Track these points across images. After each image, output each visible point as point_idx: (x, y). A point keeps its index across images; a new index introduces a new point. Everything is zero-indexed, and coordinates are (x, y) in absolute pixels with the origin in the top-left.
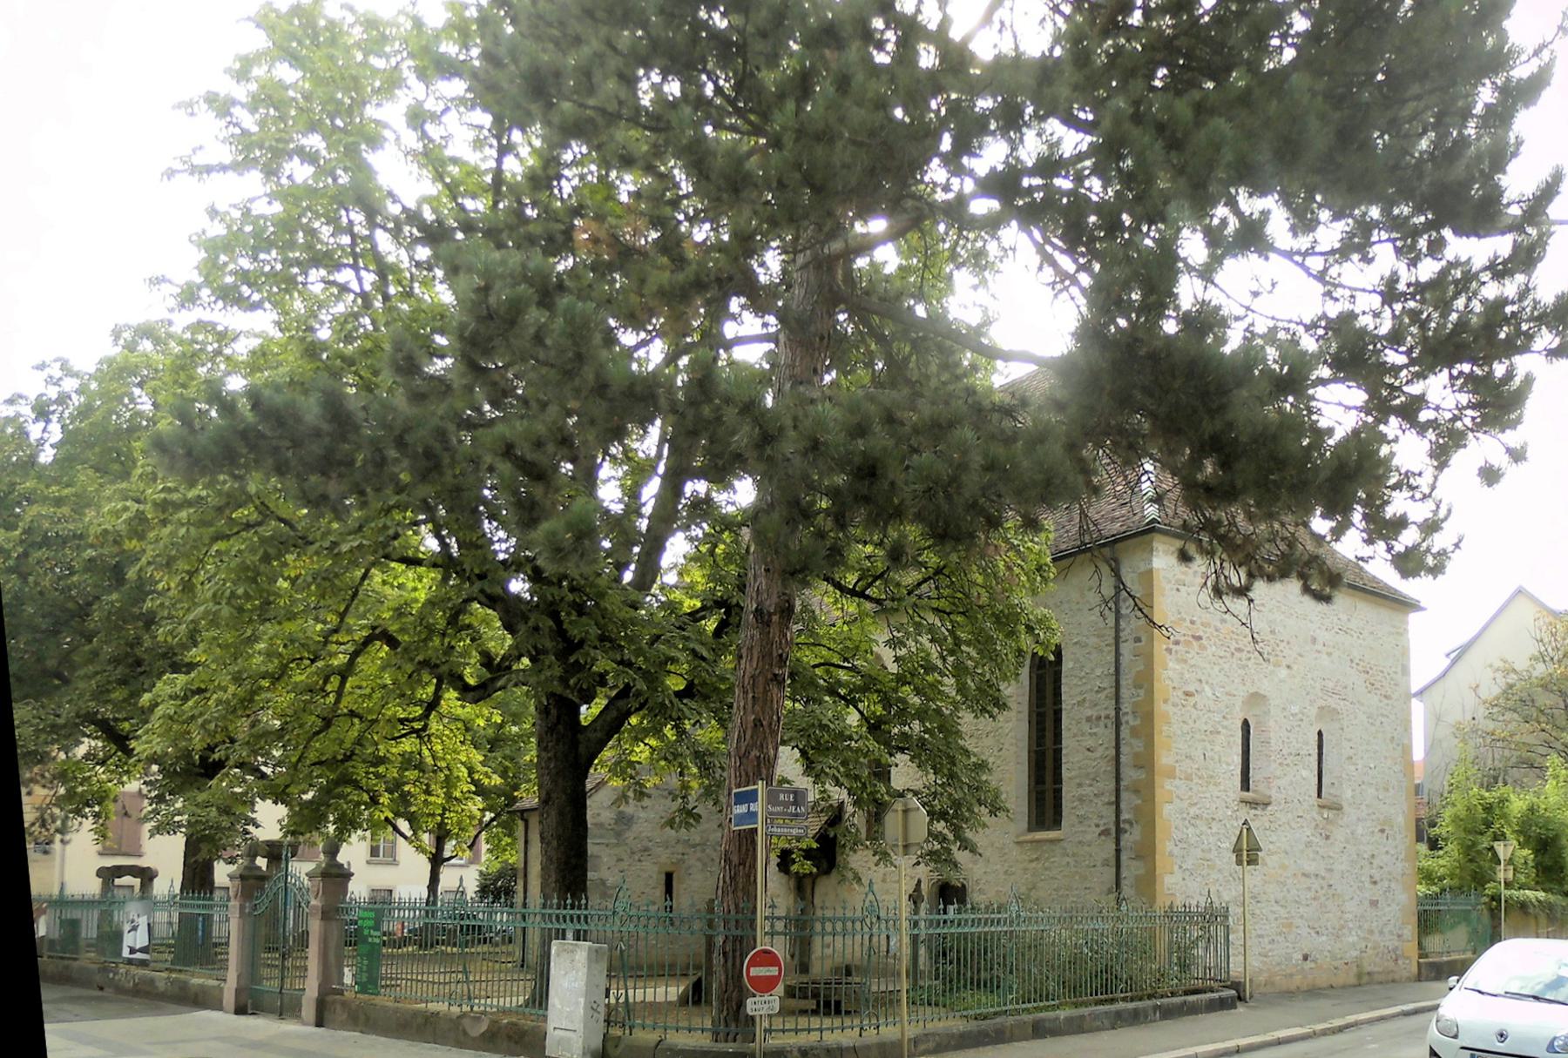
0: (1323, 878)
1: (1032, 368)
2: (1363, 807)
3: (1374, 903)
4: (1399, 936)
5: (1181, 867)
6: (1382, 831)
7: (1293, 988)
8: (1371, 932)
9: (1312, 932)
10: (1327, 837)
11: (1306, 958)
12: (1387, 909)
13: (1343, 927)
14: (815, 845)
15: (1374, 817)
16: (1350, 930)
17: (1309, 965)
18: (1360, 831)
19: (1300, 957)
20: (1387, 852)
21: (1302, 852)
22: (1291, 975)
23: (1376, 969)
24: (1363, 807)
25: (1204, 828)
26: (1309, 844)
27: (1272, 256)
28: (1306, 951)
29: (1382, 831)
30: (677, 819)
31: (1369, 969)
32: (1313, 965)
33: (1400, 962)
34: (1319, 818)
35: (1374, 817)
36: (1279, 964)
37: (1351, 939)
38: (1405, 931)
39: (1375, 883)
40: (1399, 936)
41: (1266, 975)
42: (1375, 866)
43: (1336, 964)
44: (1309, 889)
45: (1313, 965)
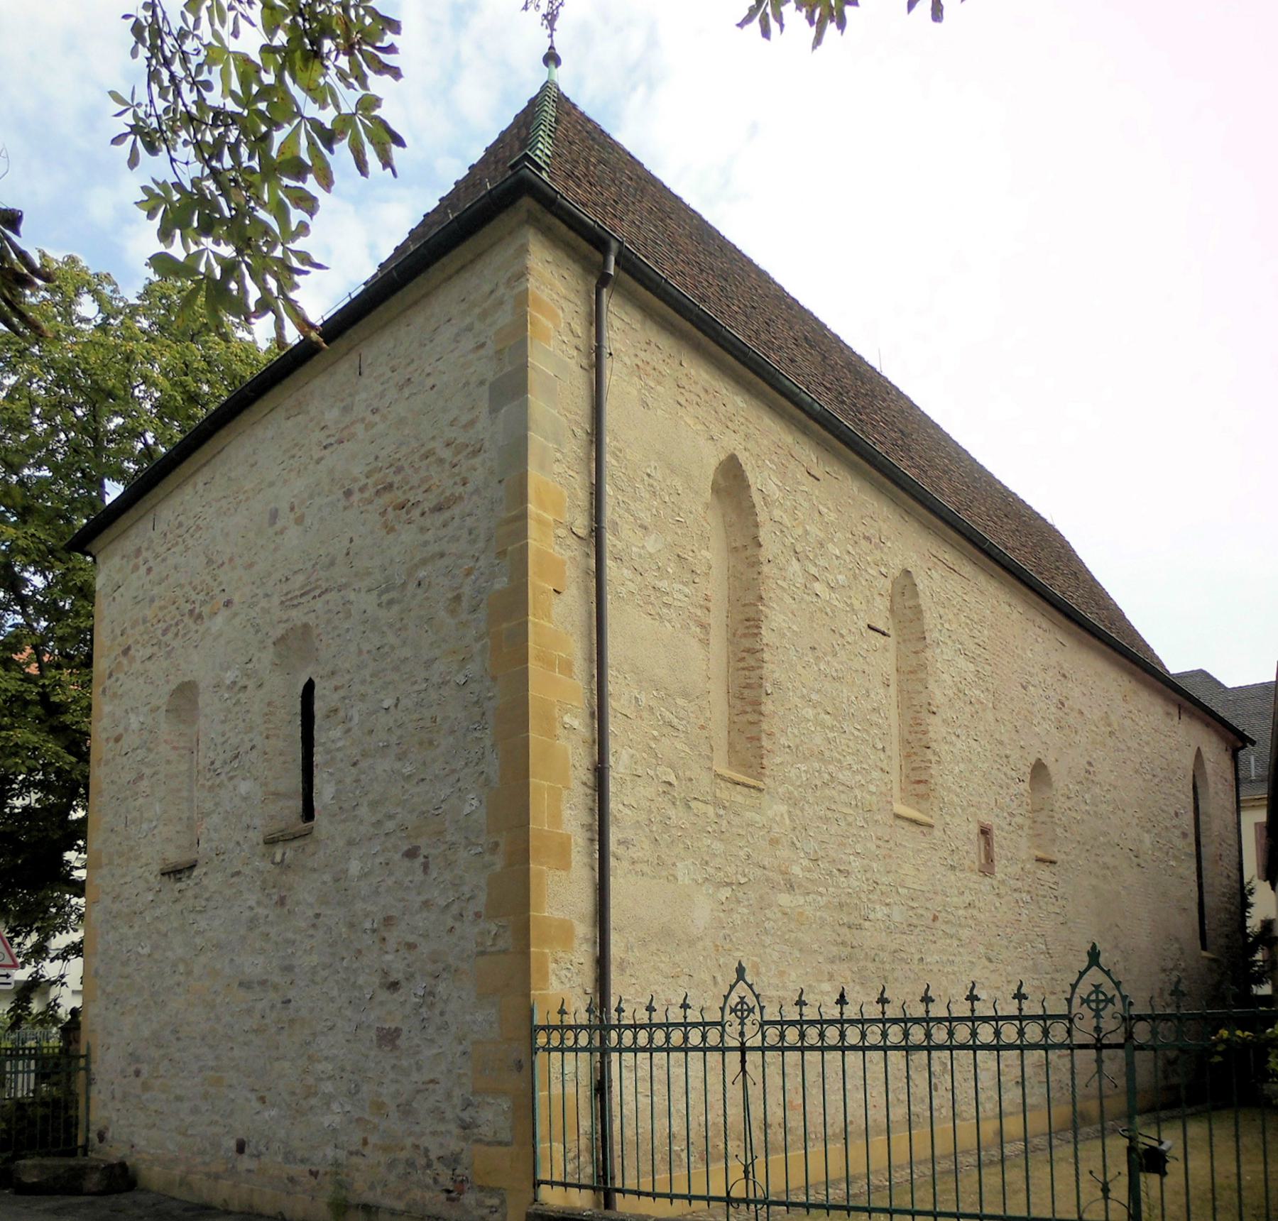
0: (276, 987)
1: (152, 84)
2: (364, 811)
3: (389, 1038)
4: (465, 1126)
5: (104, 991)
6: (411, 854)
7: (217, 1201)
8: (379, 1107)
9: (253, 1097)
10: (282, 902)
11: (241, 1147)
12: (428, 1052)
13: (310, 1093)
14: (1270, 1050)
15: (390, 825)
16: (328, 1099)
17: (245, 1163)
18: (355, 867)
19: (232, 1144)
20: (426, 904)
21: (243, 938)
22: (217, 1177)
23: (388, 1202)
24: (364, 811)
25: (125, 930)
26: (252, 923)
27: (129, 129)
28: (241, 1134)
29: (411, 854)
30: (746, 903)
31: (369, 1197)
32: (253, 1165)
33: (469, 1198)
34: (265, 865)
35: (390, 825)
36: (202, 1152)
37: (326, 1121)
38: (486, 1115)
39: (394, 986)
40: (465, 1126)
41: (182, 1168)
42: (392, 943)
43: (298, 1170)
44: (249, 1011)
45: (253, 1165)
